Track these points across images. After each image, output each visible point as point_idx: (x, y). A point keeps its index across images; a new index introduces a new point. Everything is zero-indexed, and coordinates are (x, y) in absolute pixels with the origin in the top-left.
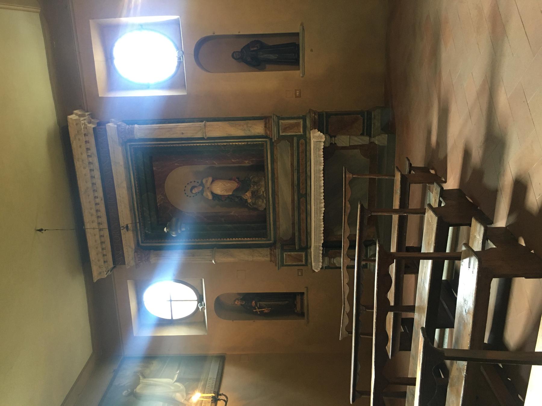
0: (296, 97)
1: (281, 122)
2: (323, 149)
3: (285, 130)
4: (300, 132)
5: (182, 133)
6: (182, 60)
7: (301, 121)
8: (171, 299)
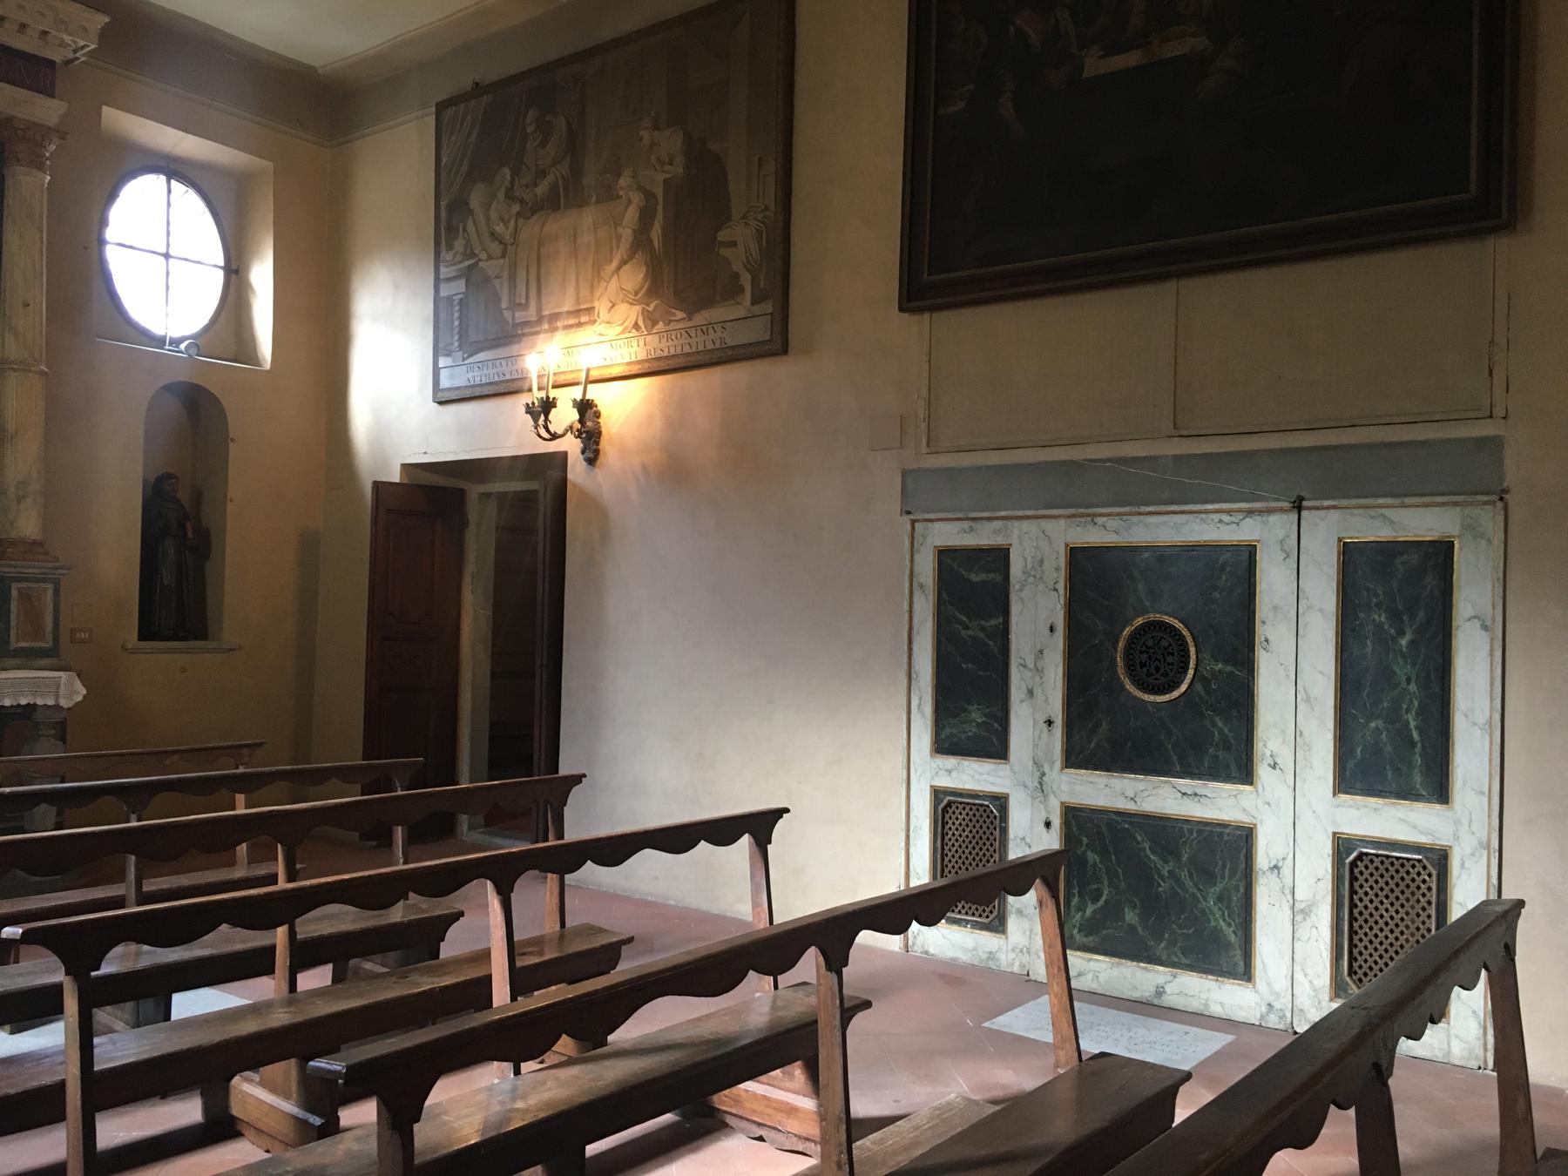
0: (71, 629)
1: (50, 587)
2: (35, 704)
3: (25, 596)
4: (17, 641)
5: (28, 305)
6: (167, 347)
7: (47, 644)
8: (172, 257)
